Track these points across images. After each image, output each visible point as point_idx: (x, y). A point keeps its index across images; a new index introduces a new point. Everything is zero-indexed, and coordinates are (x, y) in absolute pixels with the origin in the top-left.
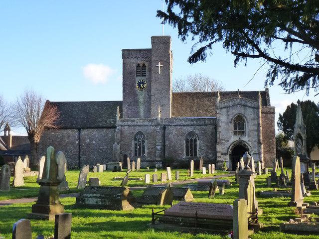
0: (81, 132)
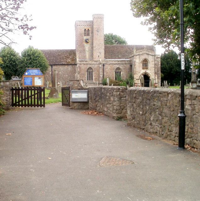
0: (53, 67)
